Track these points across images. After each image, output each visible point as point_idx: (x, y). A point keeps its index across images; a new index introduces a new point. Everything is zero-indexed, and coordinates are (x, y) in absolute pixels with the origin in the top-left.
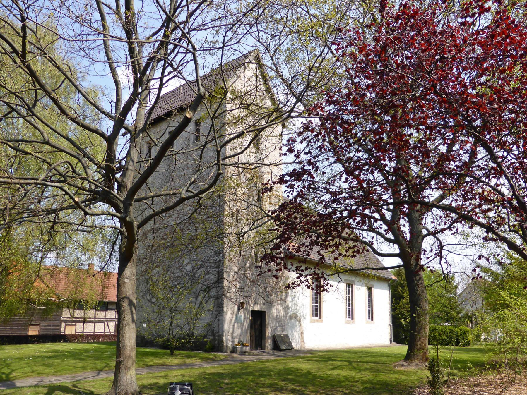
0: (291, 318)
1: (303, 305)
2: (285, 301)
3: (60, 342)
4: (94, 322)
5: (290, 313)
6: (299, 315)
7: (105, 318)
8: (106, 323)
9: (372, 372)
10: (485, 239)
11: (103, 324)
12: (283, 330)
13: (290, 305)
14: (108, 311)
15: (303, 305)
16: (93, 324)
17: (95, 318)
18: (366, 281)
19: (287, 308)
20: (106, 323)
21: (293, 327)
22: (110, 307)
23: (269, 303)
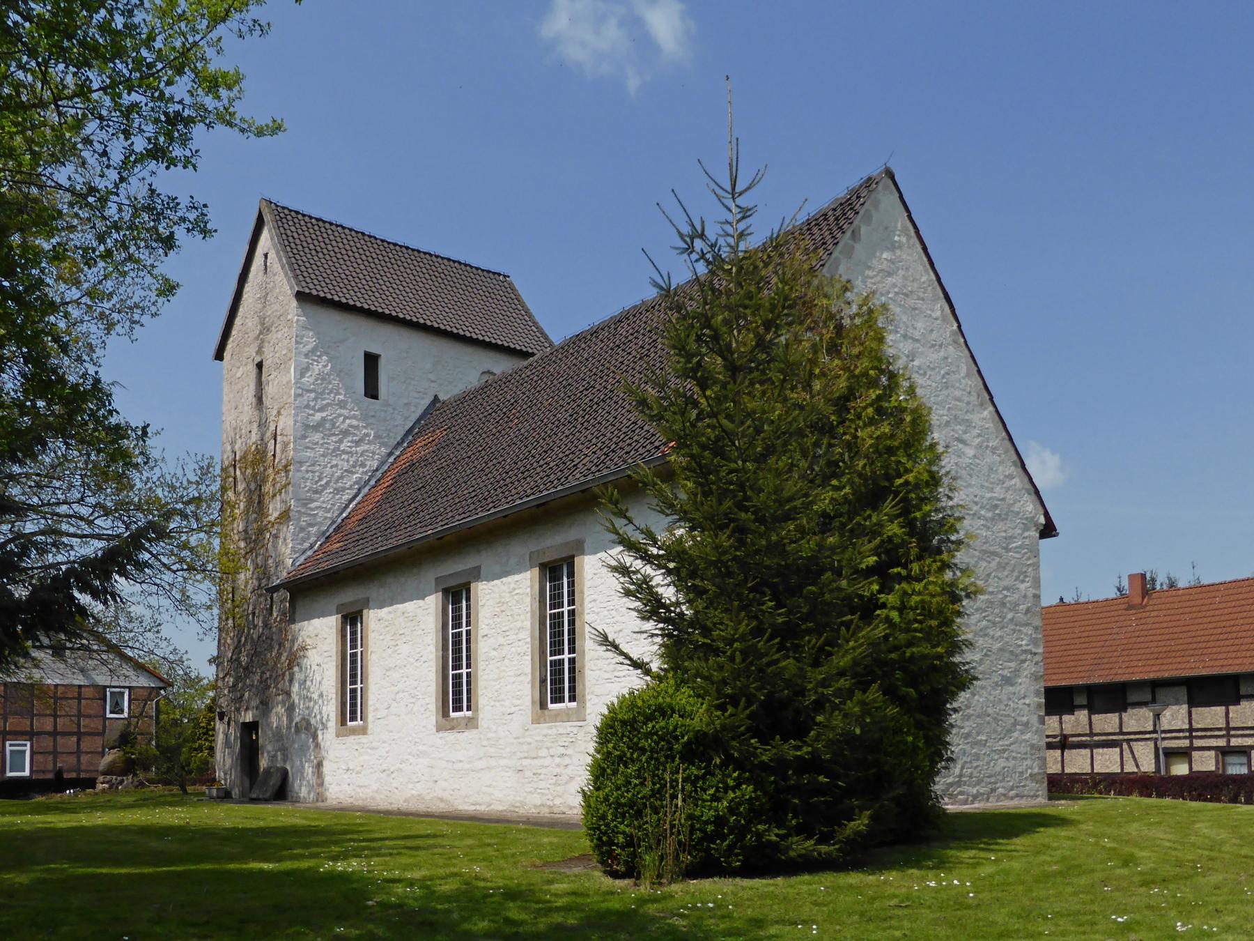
0: (298, 730)
1: (321, 696)
2: (288, 694)
3: (1234, 800)
4: (1091, 746)
5: (297, 719)
6: (313, 721)
7: (1121, 733)
8: (1125, 746)
9: (1079, 866)
10: (64, 348)
11: (1118, 750)
12: (285, 761)
13: (297, 701)
14: (1130, 711)
15: (321, 696)
16: (1088, 751)
17: (1091, 734)
18: (521, 548)
19: (291, 709)
20: (1125, 746)
21: (303, 750)
22: (1132, 698)
23: (265, 706)
